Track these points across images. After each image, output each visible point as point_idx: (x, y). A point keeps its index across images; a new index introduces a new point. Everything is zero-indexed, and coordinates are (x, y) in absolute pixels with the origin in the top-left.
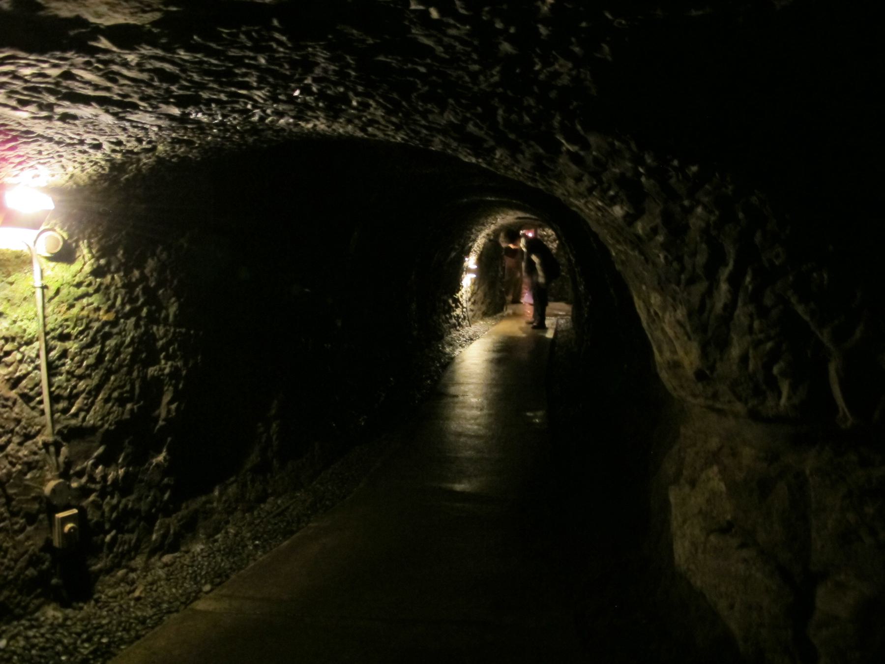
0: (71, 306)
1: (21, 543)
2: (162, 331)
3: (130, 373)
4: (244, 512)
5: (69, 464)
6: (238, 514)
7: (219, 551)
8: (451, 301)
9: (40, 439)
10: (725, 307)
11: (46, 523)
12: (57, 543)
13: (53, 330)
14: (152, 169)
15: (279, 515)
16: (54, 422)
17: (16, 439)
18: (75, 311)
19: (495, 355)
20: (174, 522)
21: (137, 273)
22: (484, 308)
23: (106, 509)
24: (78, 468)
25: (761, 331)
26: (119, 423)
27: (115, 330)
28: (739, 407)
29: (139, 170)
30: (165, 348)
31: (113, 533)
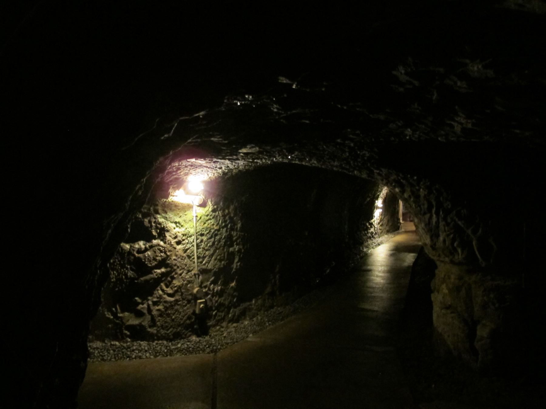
0: (205, 223)
1: (185, 310)
2: (235, 234)
3: (223, 249)
4: (265, 311)
5: (202, 283)
6: (262, 312)
7: (255, 324)
8: (368, 224)
9: (193, 272)
10: (436, 222)
11: (194, 304)
12: (197, 311)
13: (199, 232)
14: (236, 174)
15: (279, 314)
16: (198, 266)
17: (185, 272)
18: (206, 225)
19: (392, 252)
20: (237, 311)
21: (227, 211)
22: (387, 228)
23: (214, 302)
24: (205, 285)
25: (448, 231)
26: (220, 269)
27: (219, 233)
28: (447, 259)
29: (232, 174)
30: (236, 240)
31: (216, 311)
